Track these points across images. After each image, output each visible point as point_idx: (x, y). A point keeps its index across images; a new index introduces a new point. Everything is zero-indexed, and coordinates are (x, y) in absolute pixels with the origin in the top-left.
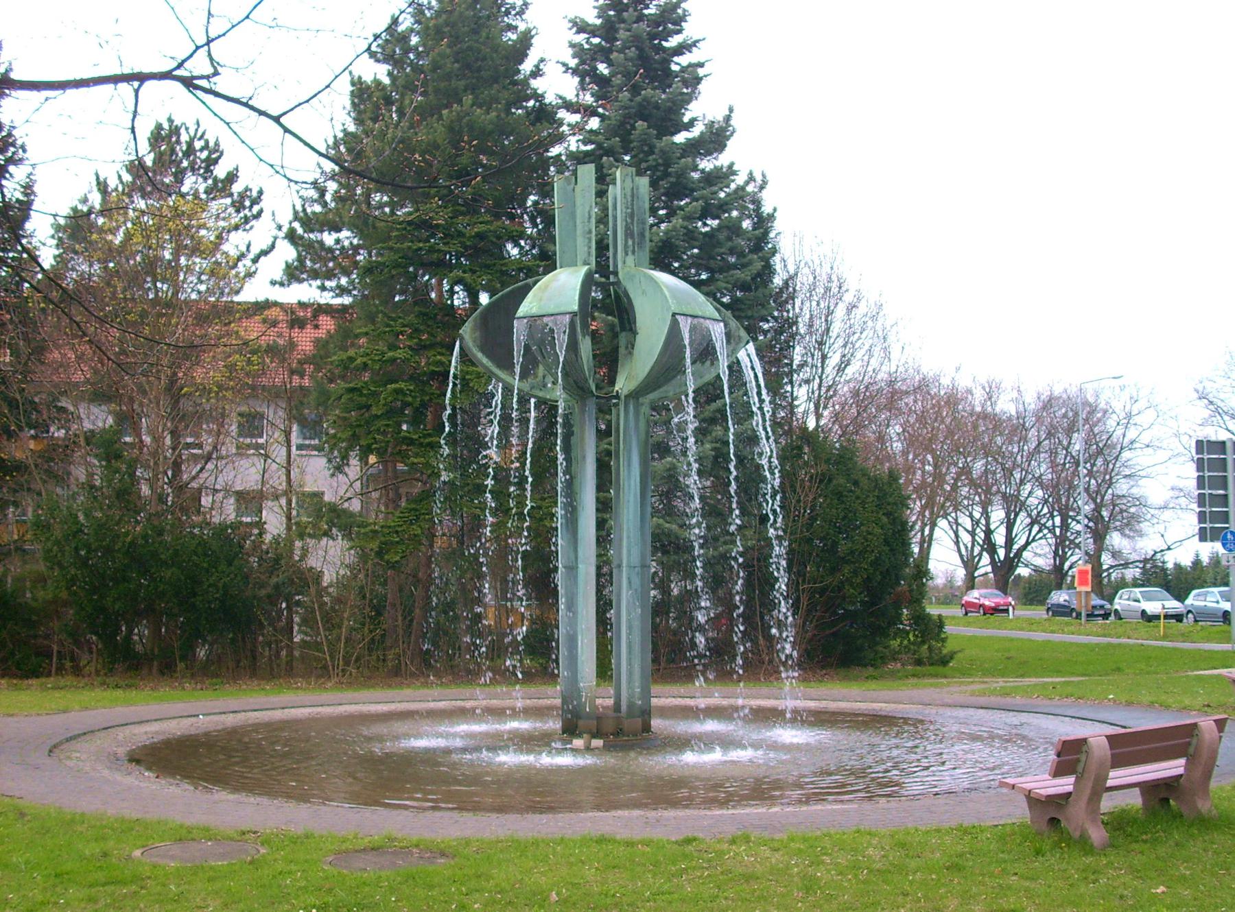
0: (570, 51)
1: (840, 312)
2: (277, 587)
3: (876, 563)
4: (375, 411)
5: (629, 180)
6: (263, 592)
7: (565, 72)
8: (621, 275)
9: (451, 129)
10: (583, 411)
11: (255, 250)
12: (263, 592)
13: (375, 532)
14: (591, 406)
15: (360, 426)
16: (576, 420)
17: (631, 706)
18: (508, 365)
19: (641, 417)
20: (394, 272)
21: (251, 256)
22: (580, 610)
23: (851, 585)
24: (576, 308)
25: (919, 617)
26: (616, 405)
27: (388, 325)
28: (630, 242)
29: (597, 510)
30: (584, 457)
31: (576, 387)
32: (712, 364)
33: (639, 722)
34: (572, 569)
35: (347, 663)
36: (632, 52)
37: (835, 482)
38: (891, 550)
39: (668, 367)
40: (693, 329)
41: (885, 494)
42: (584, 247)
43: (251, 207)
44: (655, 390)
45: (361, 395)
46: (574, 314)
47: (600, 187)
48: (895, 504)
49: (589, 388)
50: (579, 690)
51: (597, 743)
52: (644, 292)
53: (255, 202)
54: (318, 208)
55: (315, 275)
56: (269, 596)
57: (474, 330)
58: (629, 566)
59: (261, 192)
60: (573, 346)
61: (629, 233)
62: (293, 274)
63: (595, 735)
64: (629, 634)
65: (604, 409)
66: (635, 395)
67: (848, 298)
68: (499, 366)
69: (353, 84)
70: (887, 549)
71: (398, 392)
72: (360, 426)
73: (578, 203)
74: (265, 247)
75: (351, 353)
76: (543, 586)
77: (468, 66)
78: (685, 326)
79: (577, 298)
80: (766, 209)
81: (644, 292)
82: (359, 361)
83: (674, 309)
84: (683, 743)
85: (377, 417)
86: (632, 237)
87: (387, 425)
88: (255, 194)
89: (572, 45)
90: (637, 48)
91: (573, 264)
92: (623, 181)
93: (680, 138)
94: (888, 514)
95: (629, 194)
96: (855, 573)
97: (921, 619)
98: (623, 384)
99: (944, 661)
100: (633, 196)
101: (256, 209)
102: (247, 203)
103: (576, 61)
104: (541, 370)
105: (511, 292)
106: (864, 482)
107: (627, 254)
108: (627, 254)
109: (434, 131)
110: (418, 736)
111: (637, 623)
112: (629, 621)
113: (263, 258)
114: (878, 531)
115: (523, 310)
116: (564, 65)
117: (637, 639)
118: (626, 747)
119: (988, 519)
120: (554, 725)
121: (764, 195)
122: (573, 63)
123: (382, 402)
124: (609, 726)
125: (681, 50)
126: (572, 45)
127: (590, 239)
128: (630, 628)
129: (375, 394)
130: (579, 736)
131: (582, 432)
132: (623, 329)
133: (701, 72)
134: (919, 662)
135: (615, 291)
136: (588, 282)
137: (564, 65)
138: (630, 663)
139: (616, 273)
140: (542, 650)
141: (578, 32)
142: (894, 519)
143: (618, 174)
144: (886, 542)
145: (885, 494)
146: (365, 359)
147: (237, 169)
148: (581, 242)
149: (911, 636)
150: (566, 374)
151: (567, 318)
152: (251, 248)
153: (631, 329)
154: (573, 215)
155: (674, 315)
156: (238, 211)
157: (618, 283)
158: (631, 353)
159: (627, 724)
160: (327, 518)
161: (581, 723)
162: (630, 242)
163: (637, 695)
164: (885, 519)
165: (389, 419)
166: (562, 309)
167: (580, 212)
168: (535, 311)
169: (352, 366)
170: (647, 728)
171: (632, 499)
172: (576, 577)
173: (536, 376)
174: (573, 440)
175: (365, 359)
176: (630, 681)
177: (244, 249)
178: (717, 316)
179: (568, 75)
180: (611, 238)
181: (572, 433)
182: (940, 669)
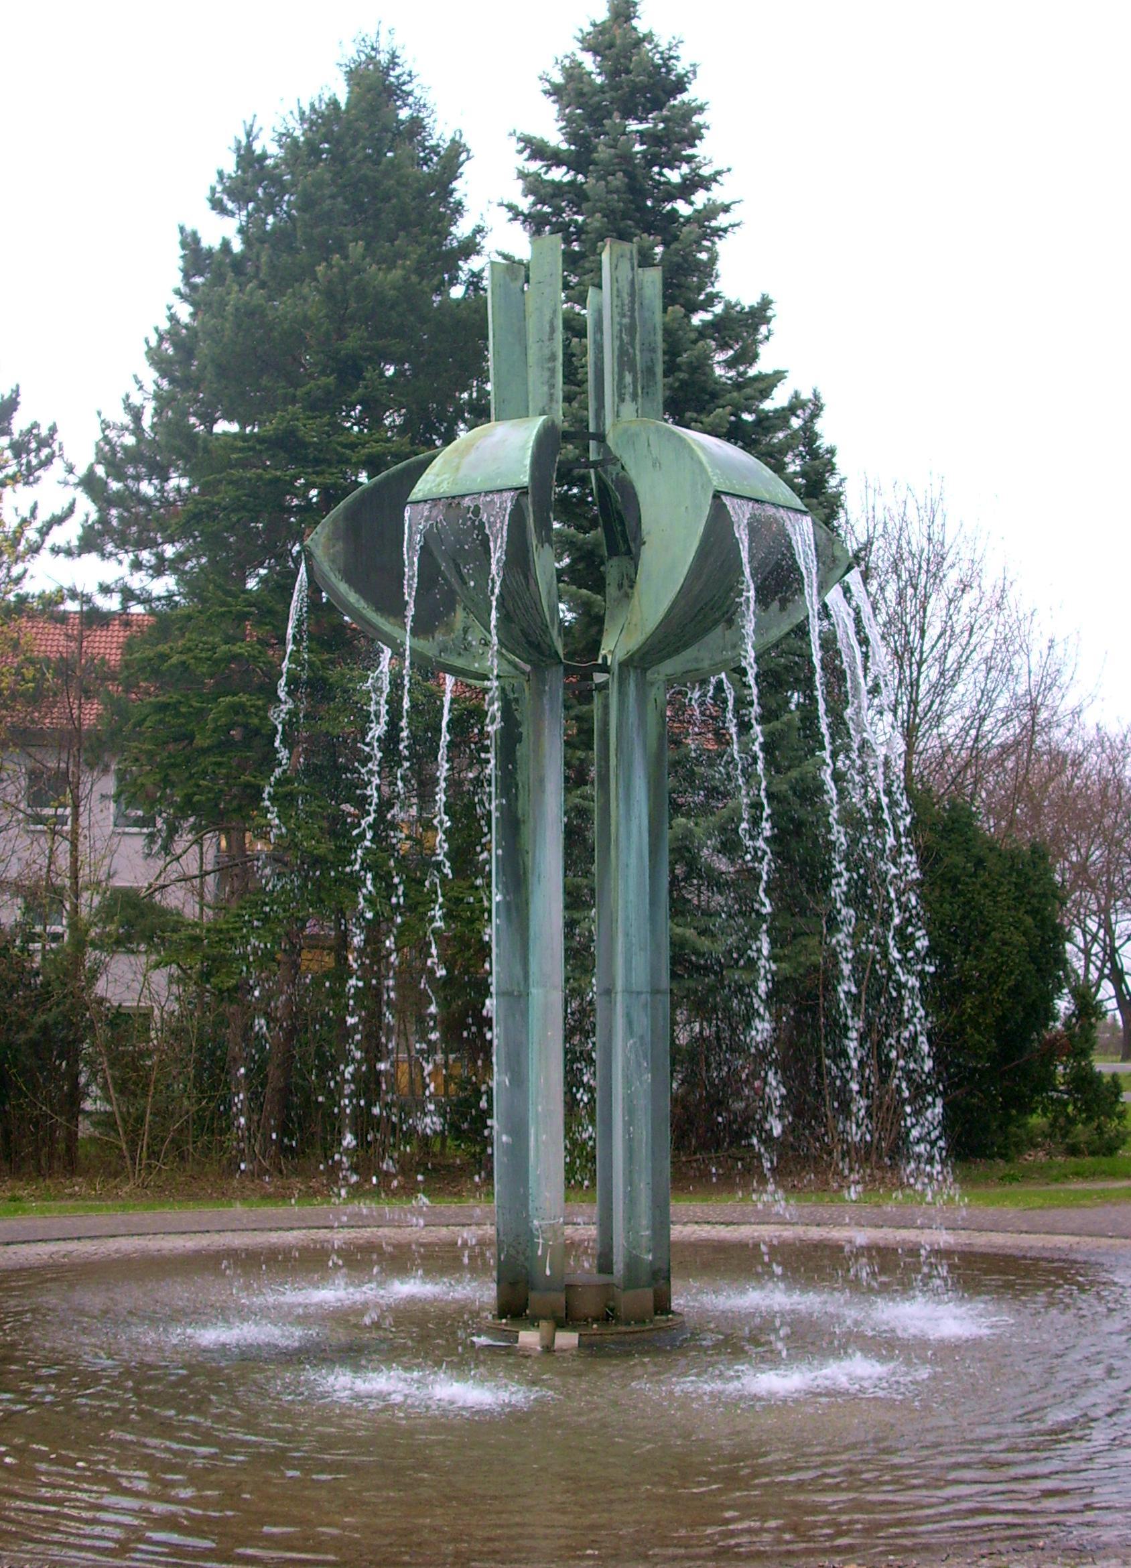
0: (520, 184)
1: (937, 605)
2: (45, 1029)
3: (1016, 991)
4: (200, 741)
5: (625, 266)
6: (22, 1037)
7: (514, 219)
8: (610, 441)
9: (329, 294)
10: (539, 694)
11: (43, 516)
12: (22, 1037)
13: (197, 939)
14: (556, 681)
15: (173, 765)
16: (524, 713)
17: (633, 1263)
18: (394, 608)
19: (651, 707)
20: (234, 518)
21: (37, 524)
22: (532, 1077)
23: (977, 1026)
24: (525, 479)
25: (1084, 1079)
26: (604, 687)
27: (223, 604)
28: (628, 378)
29: (567, 907)
30: (541, 781)
31: (525, 635)
32: (783, 608)
33: (647, 1295)
34: (517, 998)
35: (153, 1154)
36: (618, 180)
37: (947, 861)
38: (1039, 970)
39: (704, 608)
40: (754, 528)
41: (1028, 880)
42: (542, 381)
43: (38, 450)
44: (677, 651)
45: (178, 714)
46: (522, 491)
47: (567, 387)
48: (1044, 895)
49: (551, 646)
50: (531, 1233)
51: (567, 1339)
52: (656, 463)
53: (44, 443)
54: (130, 440)
55: (123, 542)
56: (33, 1044)
57: (334, 536)
58: (628, 991)
59: (53, 429)
60: (519, 558)
61: (625, 360)
62: (90, 542)
63: (564, 1321)
64: (628, 1124)
65: (582, 692)
66: (641, 661)
67: (952, 579)
68: (379, 609)
69: (184, 245)
70: (1031, 967)
71: (237, 709)
72: (173, 765)
73: (531, 306)
74: (58, 512)
75: (163, 648)
76: (466, 1032)
77: (358, 206)
78: (740, 514)
79: (528, 461)
80: (824, 443)
81: (656, 463)
82: (174, 660)
83: (718, 483)
84: (742, 1342)
85: (204, 751)
86: (633, 370)
87: (220, 764)
88: (44, 432)
89: (522, 175)
90: (626, 173)
91: (523, 413)
92: (615, 267)
93: (697, 319)
94: (1034, 912)
95: (626, 290)
96: (983, 1008)
97: (1085, 1082)
98: (616, 645)
99: (1110, 1149)
100: (632, 295)
101: (45, 452)
102: (33, 445)
103: (531, 199)
104: (460, 617)
105: (404, 470)
106: (991, 861)
107: (622, 399)
108: (622, 399)
109: (304, 303)
110: (224, 1314)
111: (643, 1103)
112: (629, 1099)
113: (55, 528)
114: (1018, 939)
115: (424, 487)
116: (511, 207)
117: (643, 1133)
118: (625, 1350)
119: (1109, 931)
120: (481, 1292)
121: (819, 426)
122: (525, 204)
123: (211, 726)
124: (589, 1305)
125: (687, 188)
126: (522, 175)
127: (552, 371)
128: (630, 1111)
129: (201, 714)
130: (533, 1322)
131: (538, 734)
132: (613, 551)
133: (722, 220)
134: (1073, 1151)
135: (599, 479)
136: (548, 442)
137: (511, 207)
138: (629, 1182)
139: (600, 437)
140: (460, 1153)
141: (532, 157)
142: (1043, 920)
143: (605, 257)
144: (1034, 960)
145: (1028, 880)
146: (184, 658)
147: (16, 392)
148: (535, 378)
149: (1070, 1108)
150: (506, 618)
151: (508, 499)
152: (39, 512)
153: (629, 552)
154: (521, 336)
155: (717, 495)
156: (17, 456)
157: (609, 459)
158: (627, 596)
159: (626, 1301)
160: (136, 920)
161: (533, 1296)
162: (628, 378)
163: (644, 1241)
164: (1029, 920)
165: (222, 754)
166: (499, 483)
167: (534, 327)
168: (446, 488)
169: (165, 667)
170: (662, 1305)
171: (633, 861)
172: (525, 1014)
173: (449, 628)
174: (521, 750)
175: (184, 658)
176: (630, 1217)
177: (27, 514)
178: (797, 503)
179: (517, 225)
180: (590, 369)
181: (519, 738)
182: (1104, 1162)
